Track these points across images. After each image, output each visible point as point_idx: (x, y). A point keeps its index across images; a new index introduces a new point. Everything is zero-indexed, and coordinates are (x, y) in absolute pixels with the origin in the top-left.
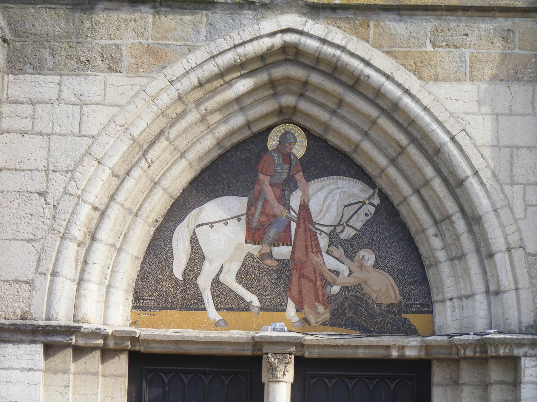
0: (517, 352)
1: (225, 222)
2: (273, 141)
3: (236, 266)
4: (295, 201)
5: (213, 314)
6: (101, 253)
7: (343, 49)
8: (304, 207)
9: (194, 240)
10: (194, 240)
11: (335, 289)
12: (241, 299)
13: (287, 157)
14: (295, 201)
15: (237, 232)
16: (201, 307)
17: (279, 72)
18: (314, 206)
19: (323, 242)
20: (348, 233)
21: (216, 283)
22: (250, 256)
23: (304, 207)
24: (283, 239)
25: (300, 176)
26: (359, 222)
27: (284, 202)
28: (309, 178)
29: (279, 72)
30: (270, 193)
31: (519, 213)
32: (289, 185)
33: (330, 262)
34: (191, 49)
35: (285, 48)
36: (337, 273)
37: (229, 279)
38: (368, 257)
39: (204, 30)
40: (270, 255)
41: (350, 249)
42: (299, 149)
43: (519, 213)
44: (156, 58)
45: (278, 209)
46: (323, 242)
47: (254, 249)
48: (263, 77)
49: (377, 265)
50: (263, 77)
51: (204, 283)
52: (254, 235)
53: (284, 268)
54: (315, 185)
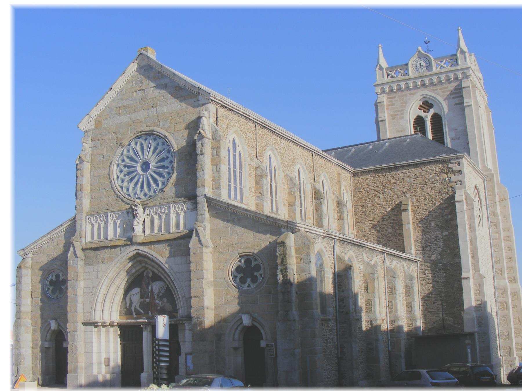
0: (184, 322)
1: (136, 294)
2: (145, 274)
3: (139, 304)
4: (150, 288)
5: (135, 316)
6: (107, 305)
7: (147, 253)
8: (152, 289)
9: (130, 299)
10: (130, 299)
11: (159, 308)
12: (140, 312)
13: (148, 277)
14: (150, 288)
15: (138, 296)
16: (132, 314)
17: (138, 259)
18: (154, 288)
19: (156, 297)
20: (161, 295)
21: (135, 308)
22: (141, 302)
23: (152, 289)
24: (148, 297)
25: (151, 282)
26: (163, 292)
27: (148, 288)
28: (153, 282)
29: (138, 259)
30: (145, 286)
31: (184, 288)
32: (148, 284)
33: (157, 302)
34: (118, 256)
35: (137, 253)
36: (159, 304)
37: (138, 307)
38: (165, 300)
39: (120, 251)
40: (145, 301)
41: (161, 298)
42: (150, 275)
43: (184, 288)
44: (111, 259)
45: (146, 290)
46: (156, 297)
47: (142, 300)
48: (135, 261)
49: (167, 302)
50: (135, 261)
51: (133, 309)
52: (142, 297)
53: (149, 303)
54: (154, 283)
